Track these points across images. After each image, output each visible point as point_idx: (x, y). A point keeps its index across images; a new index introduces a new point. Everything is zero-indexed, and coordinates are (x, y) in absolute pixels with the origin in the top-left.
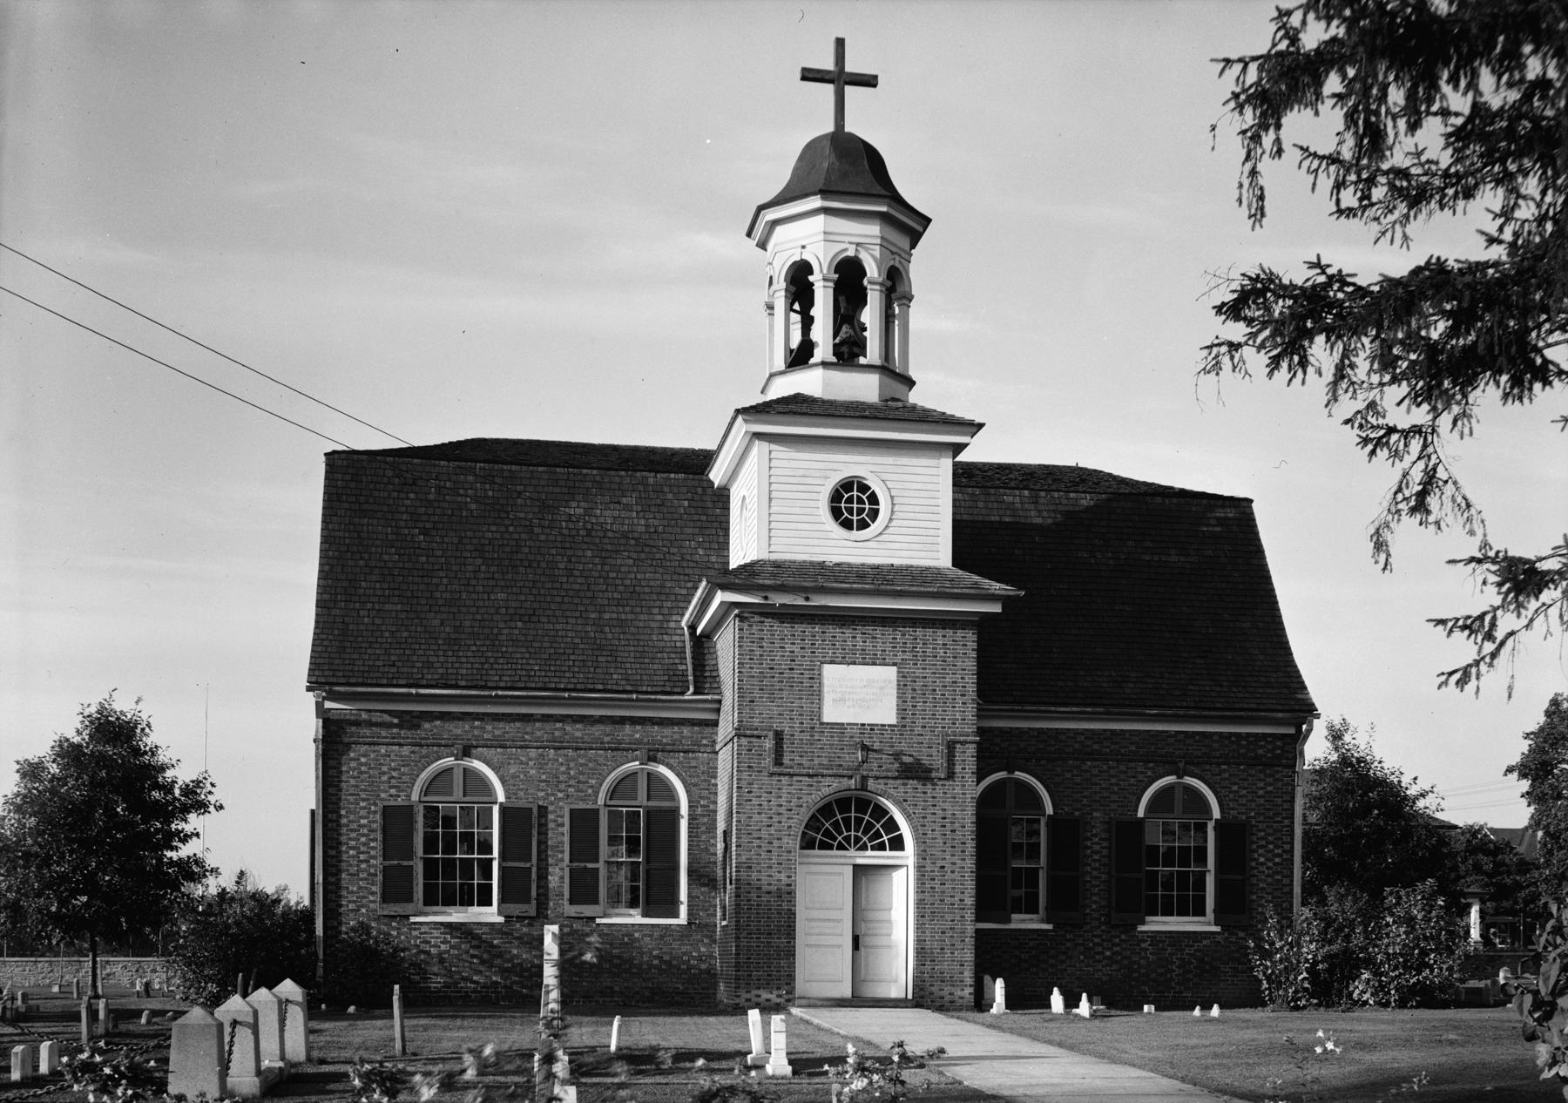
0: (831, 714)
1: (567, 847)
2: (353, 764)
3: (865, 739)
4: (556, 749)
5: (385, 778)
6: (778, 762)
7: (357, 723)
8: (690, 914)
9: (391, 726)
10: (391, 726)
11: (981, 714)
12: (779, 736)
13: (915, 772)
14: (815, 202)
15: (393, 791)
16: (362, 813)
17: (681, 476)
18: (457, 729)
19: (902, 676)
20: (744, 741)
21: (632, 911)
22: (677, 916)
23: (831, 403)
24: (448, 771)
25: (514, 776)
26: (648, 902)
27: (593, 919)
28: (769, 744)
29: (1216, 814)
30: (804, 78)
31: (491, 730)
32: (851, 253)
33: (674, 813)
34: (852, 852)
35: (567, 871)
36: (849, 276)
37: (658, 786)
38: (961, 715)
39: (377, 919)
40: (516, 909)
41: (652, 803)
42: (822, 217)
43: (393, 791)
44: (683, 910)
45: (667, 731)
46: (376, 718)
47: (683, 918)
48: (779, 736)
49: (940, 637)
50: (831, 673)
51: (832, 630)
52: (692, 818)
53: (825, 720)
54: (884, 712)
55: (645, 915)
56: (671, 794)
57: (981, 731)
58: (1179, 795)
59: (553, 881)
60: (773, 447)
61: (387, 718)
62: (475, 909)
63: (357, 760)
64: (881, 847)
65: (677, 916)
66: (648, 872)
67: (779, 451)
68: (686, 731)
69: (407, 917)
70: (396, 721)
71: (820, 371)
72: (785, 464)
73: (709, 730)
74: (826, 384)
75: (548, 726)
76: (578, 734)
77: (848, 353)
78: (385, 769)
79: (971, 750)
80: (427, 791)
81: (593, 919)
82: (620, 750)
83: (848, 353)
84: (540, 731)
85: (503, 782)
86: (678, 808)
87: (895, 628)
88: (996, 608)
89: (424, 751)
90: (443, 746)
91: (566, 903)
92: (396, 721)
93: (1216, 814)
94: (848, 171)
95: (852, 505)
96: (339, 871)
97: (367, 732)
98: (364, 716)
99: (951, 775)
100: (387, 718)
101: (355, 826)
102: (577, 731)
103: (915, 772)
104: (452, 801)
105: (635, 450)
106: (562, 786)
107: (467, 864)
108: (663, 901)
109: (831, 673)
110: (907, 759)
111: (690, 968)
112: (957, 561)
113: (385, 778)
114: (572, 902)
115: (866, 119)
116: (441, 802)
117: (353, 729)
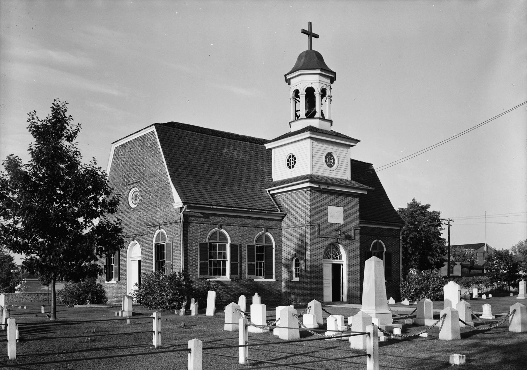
0: (330, 220)
1: (247, 257)
2: (191, 229)
3: (337, 228)
4: (244, 227)
5: (199, 234)
6: (319, 234)
7: (191, 216)
8: (276, 278)
9: (201, 217)
10: (201, 217)
11: (360, 223)
12: (319, 225)
13: (348, 237)
14: (318, 71)
15: (202, 239)
16: (194, 245)
17: (248, 143)
18: (218, 219)
19: (344, 210)
20: (312, 227)
21: (261, 277)
22: (272, 278)
23: (318, 129)
24: (215, 233)
25: (233, 235)
26: (266, 274)
27: (253, 279)
28: (317, 228)
29: (385, 250)
30: (303, 32)
31: (228, 220)
32: (324, 87)
33: (271, 247)
34: (331, 260)
35: (247, 265)
36: (310, 92)
37: (268, 239)
38: (356, 222)
39: (198, 280)
40: (235, 277)
41: (266, 244)
42: (318, 75)
43: (202, 239)
44: (274, 276)
45: (270, 222)
46: (197, 214)
47: (274, 279)
48: (319, 225)
49: (352, 199)
50: (330, 208)
51: (330, 196)
52: (276, 249)
53: (329, 222)
54: (341, 221)
55: (265, 278)
56: (270, 242)
57: (360, 227)
58: (378, 244)
59: (243, 267)
60: (313, 141)
61: (200, 215)
62: (222, 276)
63: (192, 227)
64: (337, 259)
65: (272, 278)
66: (266, 265)
67: (315, 143)
68: (274, 222)
69: (206, 279)
70: (202, 216)
71: (318, 120)
72: (316, 147)
73: (279, 222)
74: (319, 124)
75: (241, 219)
76: (248, 222)
77: (310, 115)
78: (199, 231)
79: (358, 232)
80: (210, 239)
81: (253, 279)
82: (259, 227)
83: (310, 115)
84: (239, 221)
85: (230, 237)
86: (272, 246)
87: (334, 195)
88: (366, 193)
89: (210, 226)
90: (214, 224)
91: (247, 274)
92: (202, 216)
93: (385, 250)
94: (312, 61)
95: (329, 159)
96: (188, 264)
97: (194, 219)
98: (193, 214)
99: (355, 239)
100: (200, 215)
101: (191, 250)
102: (248, 221)
103: (348, 237)
104: (217, 241)
105: (184, 125)
106: (245, 238)
107: (219, 262)
108: (269, 275)
109: (330, 208)
110: (346, 234)
111: (202, 291)
112: (352, 178)
113: (199, 234)
114: (248, 274)
115: (317, 46)
116: (213, 242)
117: (190, 218)
